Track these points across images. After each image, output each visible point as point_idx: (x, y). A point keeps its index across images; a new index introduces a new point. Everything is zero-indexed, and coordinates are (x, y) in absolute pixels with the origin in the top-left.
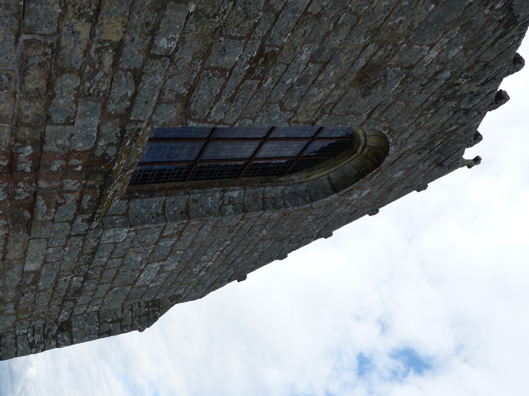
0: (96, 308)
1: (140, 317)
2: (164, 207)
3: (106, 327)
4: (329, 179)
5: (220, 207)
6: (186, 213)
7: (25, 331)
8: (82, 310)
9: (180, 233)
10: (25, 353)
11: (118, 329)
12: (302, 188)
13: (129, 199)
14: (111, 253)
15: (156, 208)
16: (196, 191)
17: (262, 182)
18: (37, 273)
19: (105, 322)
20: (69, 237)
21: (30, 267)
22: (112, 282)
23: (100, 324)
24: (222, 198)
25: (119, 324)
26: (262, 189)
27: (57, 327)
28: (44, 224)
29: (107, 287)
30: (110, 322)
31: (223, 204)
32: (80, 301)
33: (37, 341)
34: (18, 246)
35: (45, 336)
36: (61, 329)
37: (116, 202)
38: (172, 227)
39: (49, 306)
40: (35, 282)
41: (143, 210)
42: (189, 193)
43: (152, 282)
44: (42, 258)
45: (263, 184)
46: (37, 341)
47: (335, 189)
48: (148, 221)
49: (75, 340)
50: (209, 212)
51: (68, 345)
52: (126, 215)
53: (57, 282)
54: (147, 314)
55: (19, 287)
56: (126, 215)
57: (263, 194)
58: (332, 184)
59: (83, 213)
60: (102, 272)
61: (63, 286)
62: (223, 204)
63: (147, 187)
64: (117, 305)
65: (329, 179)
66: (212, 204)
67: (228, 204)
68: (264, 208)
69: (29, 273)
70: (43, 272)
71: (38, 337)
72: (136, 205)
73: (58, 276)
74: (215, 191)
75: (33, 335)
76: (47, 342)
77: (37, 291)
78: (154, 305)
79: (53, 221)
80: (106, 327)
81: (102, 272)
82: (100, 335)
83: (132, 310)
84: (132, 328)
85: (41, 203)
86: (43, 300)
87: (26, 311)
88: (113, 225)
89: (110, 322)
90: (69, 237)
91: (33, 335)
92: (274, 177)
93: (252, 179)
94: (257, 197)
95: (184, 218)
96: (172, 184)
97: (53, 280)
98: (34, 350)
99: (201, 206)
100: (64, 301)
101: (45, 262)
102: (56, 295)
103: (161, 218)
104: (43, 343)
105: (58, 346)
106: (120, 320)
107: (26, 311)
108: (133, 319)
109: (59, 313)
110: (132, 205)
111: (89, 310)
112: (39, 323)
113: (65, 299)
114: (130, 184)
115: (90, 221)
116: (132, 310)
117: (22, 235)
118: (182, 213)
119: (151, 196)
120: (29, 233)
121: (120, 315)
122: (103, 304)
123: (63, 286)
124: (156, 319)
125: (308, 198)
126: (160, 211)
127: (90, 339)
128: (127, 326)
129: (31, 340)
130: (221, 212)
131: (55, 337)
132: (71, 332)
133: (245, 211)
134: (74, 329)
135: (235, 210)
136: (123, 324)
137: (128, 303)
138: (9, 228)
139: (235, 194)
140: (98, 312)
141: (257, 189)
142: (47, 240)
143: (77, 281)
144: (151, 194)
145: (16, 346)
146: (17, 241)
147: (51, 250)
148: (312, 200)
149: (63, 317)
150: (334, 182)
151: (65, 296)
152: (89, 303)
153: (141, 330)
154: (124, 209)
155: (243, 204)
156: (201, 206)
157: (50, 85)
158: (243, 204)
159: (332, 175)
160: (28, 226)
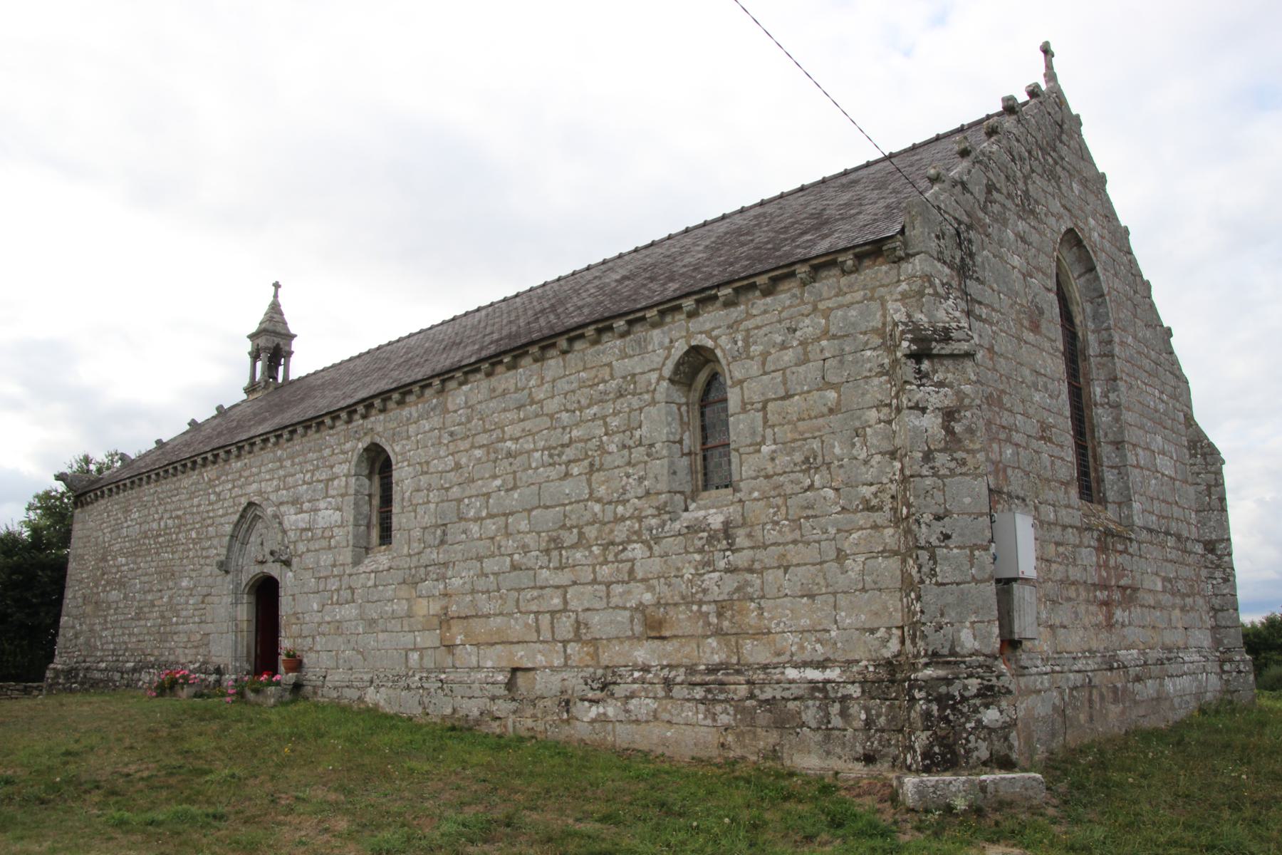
0: (1193, 515)
1: (1207, 464)
2: (1112, 467)
3: (1215, 503)
4: (1080, 276)
5: (1111, 407)
6: (1118, 444)
7: (1210, 586)
8: (1193, 529)
9: (1134, 445)
10: (1234, 587)
11: (1218, 489)
12: (1089, 308)
13: (1107, 502)
14: (1149, 513)
15: (1113, 475)
16: (1096, 434)
17: (1085, 360)
18: (1165, 579)
19: (1209, 504)
20: (1140, 556)
21: (1159, 587)
22: (1171, 504)
23: (1211, 509)
24: (1102, 405)
25: (1213, 489)
26: (1092, 359)
27: (1210, 555)
28: (1133, 578)
29: (1175, 508)
30: (1210, 498)
31: (1108, 403)
32: (1185, 534)
33: (1222, 575)
34: (1146, 596)
35: (1218, 566)
36: (1212, 551)
37: (1110, 514)
38: (1131, 459)
39: (1188, 565)
40: (1170, 581)
41: (1115, 488)
42: (1099, 443)
43: (1171, 458)
44: (1154, 577)
45: (1086, 359)
46: (1222, 575)
47: (1091, 269)
48: (1126, 484)
49: (1226, 537)
50: (1117, 419)
51: (1230, 544)
52: (1120, 504)
53: (1171, 561)
54: (1204, 455)
55: (1173, 594)
56: (1120, 504)
57: (1097, 356)
58: (1086, 273)
59: (1126, 548)
60: (1164, 518)
61: (1174, 555)
62: (1108, 403)
63: (1094, 485)
64: (1191, 490)
65: (1080, 276)
66: (1108, 416)
67: (1108, 397)
68: (1111, 355)
69: (1164, 587)
70: (1163, 574)
71: (1218, 574)
72: (1111, 495)
73: (1167, 560)
74: (1096, 414)
75: (1215, 579)
76: (1224, 565)
77: (1176, 578)
78: (1195, 448)
79: (1131, 571)
80: (1215, 503)
81: (1164, 518)
82: (1224, 510)
83: (1198, 474)
84: (1219, 474)
85: (1122, 583)
86: (1185, 572)
87: (1192, 586)
88: (1130, 517)
89: (1210, 498)
90: (1140, 556)
91: (1215, 579)
92: (1079, 345)
93: (1081, 371)
94: (1099, 363)
95: (1123, 447)
96: (1091, 460)
97: (1169, 565)
98: (1231, 579)
99: (1110, 427)
100: (1186, 552)
101: (1157, 574)
102: (1181, 559)
103: (1123, 470)
104: (1224, 570)
105: (1230, 554)
106: (1209, 486)
107: (1192, 586)
108: (1209, 472)
109: (1196, 554)
110: (1110, 499)
111: (1195, 522)
112: (1204, 573)
113: (1185, 551)
114: (1091, 501)
115: (1131, 540)
116: (1198, 474)
117: (1140, 594)
118: (1118, 449)
119: (1103, 481)
120: (1138, 589)
121: (1203, 487)
122: (1189, 508)
123: (1174, 555)
124: (1211, 445)
125: (1100, 300)
126: (1116, 471)
127: (1227, 520)
128: (1216, 479)
129: (1220, 581)
130: (1117, 406)
131: (1220, 557)
132: (1216, 541)
133: (1115, 379)
134: (1214, 537)
135: (1115, 390)
136: (1213, 483)
137: (1190, 480)
138: (894, 510)
139: (1098, 390)
140: (1197, 512)
141: (1093, 365)
142: (1142, 574)
143: (1171, 542)
144: (1100, 480)
145: (1224, 595)
146: (1143, 598)
147: (1149, 570)
148: (1102, 295)
149: (1199, 549)
150: (1083, 270)
151: (1182, 551)
152: (1189, 524)
153: (1223, 462)
154: (1115, 506)
155: (1107, 381)
156: (1110, 427)
157: (1073, 583)
158: (1107, 381)
159: (1076, 275)
160: (1135, 590)
